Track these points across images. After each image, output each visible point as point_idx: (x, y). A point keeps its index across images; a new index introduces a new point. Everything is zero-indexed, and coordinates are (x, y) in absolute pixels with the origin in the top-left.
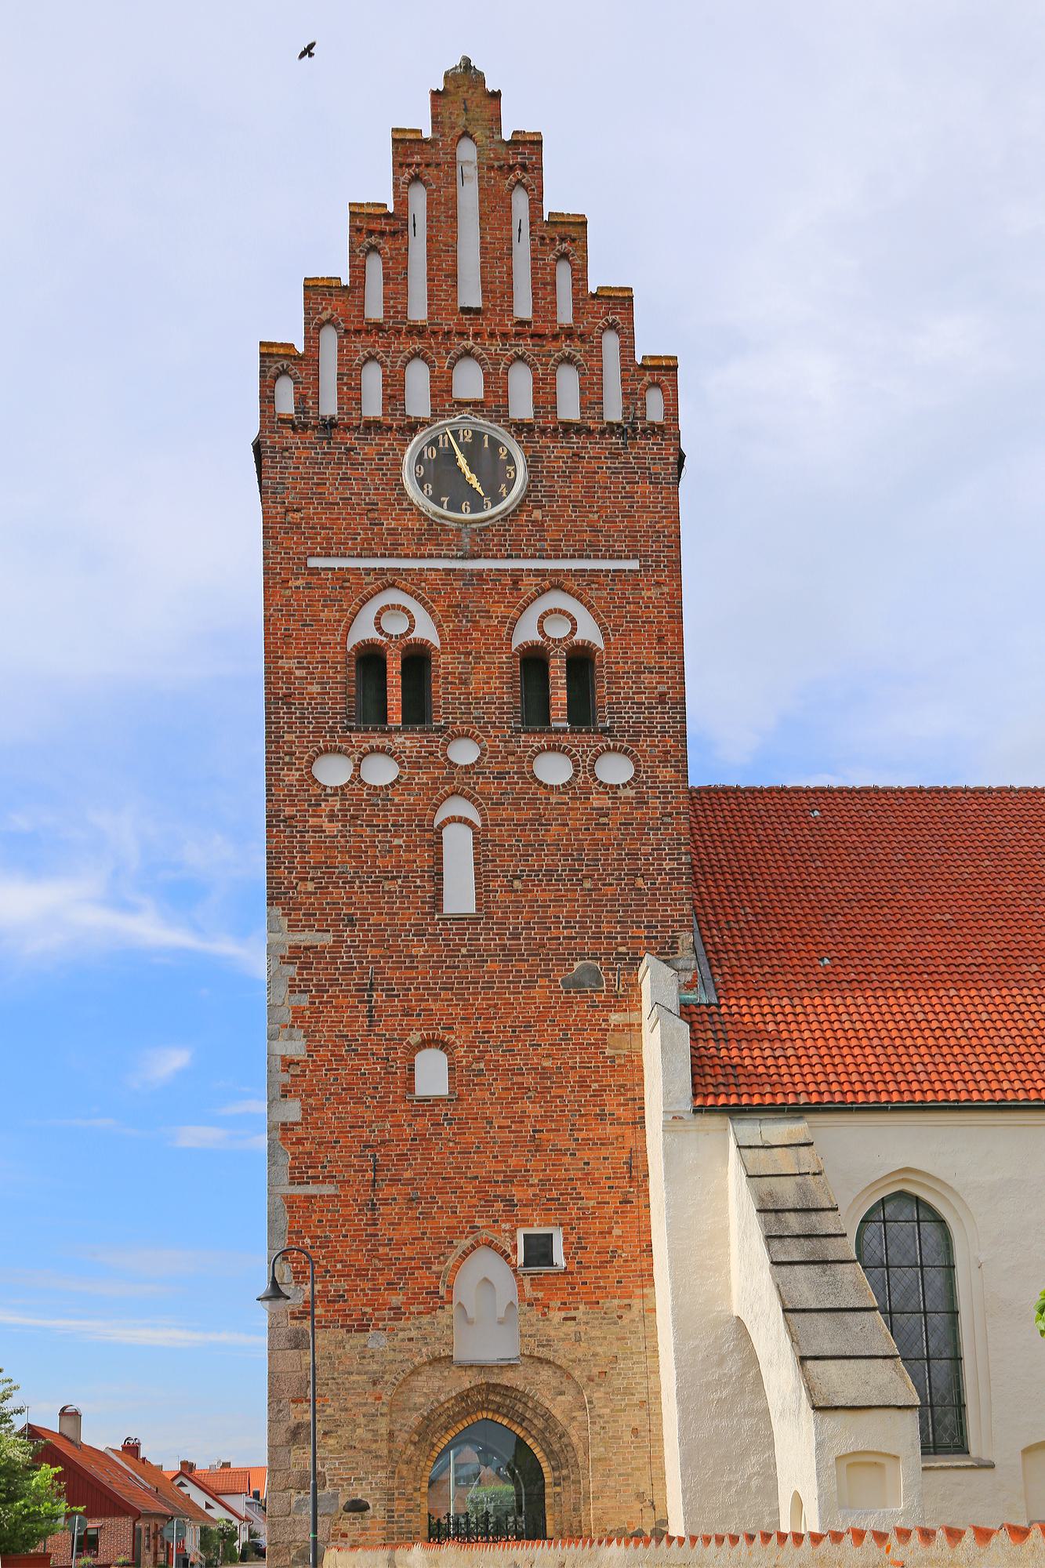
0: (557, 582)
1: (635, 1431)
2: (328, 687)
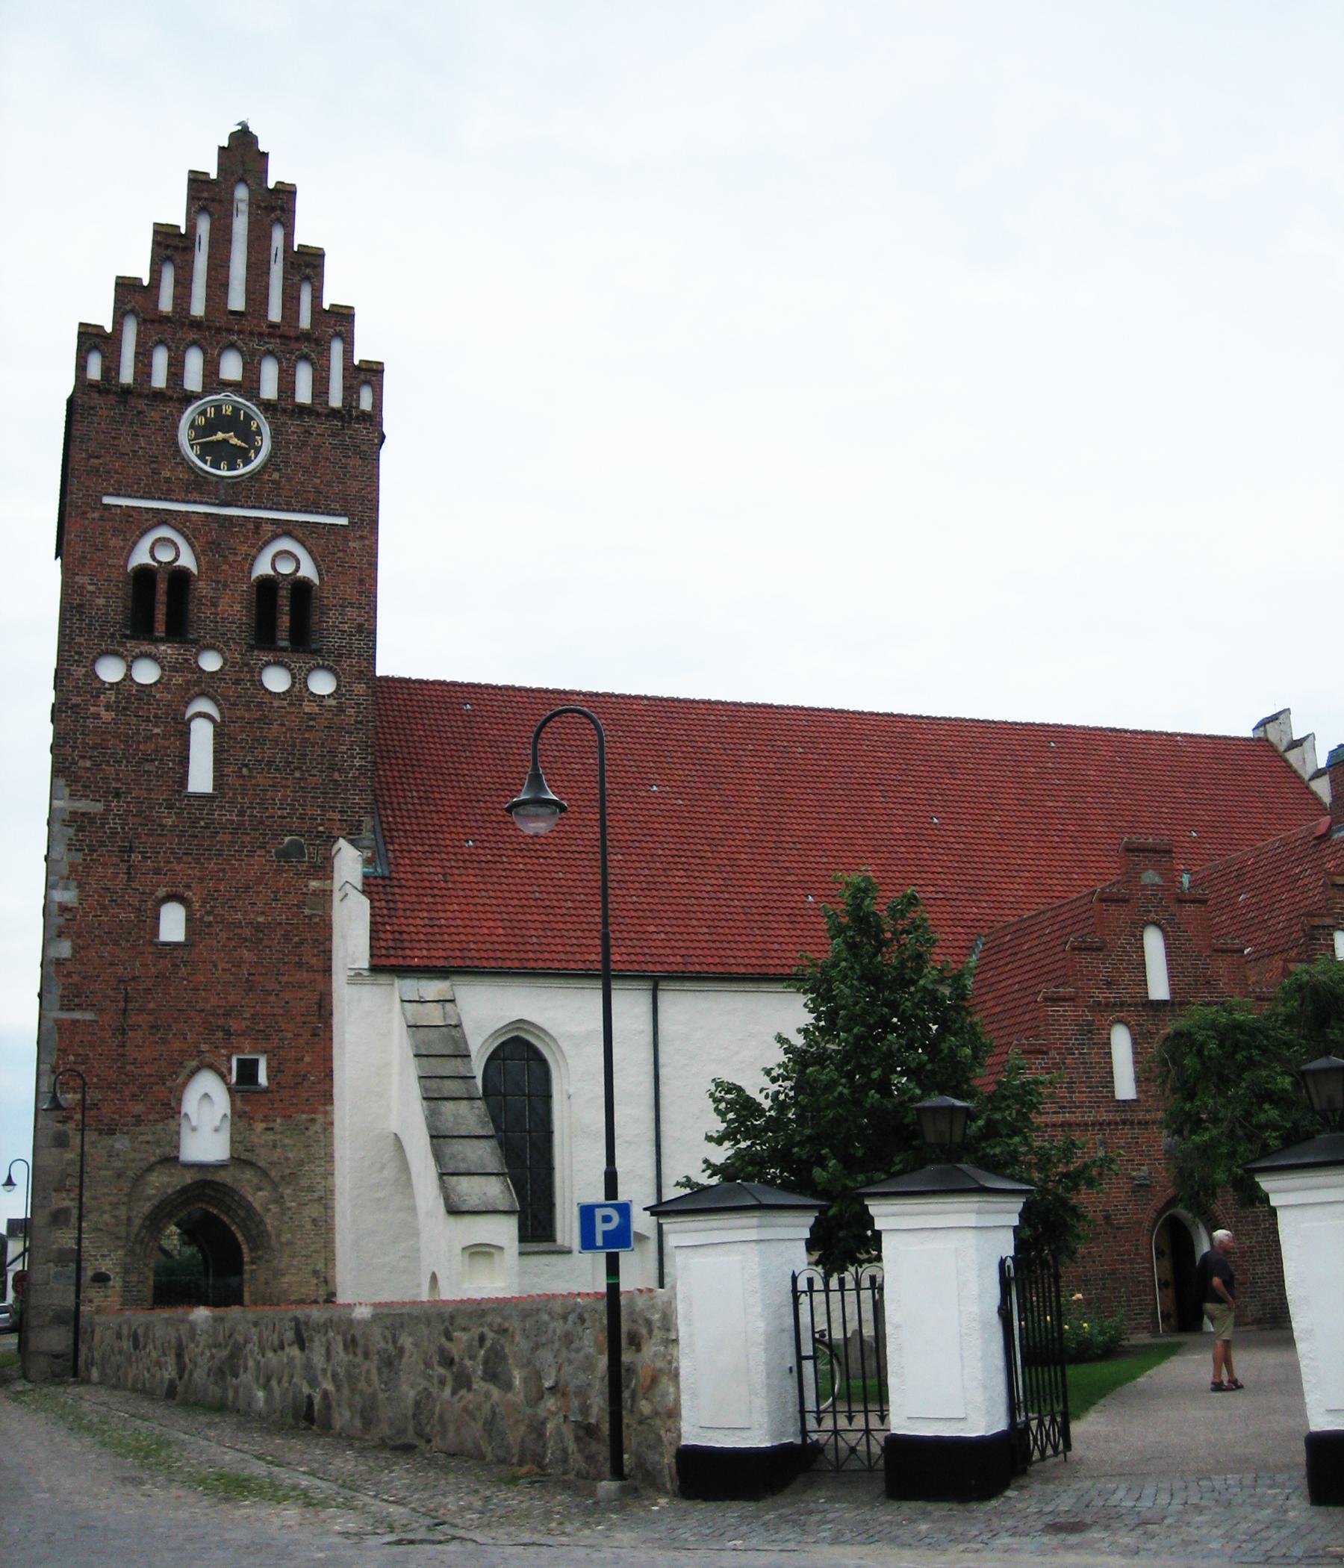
0: (286, 530)
1: (314, 1221)
2: (109, 603)
